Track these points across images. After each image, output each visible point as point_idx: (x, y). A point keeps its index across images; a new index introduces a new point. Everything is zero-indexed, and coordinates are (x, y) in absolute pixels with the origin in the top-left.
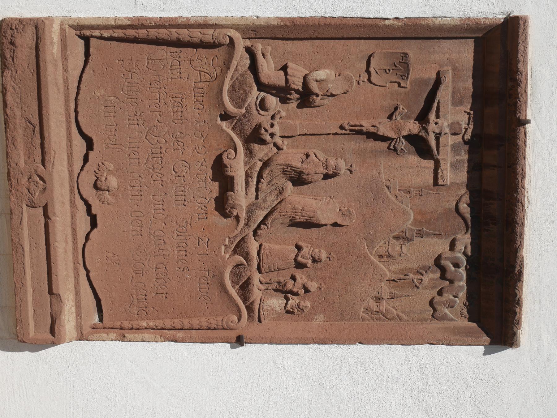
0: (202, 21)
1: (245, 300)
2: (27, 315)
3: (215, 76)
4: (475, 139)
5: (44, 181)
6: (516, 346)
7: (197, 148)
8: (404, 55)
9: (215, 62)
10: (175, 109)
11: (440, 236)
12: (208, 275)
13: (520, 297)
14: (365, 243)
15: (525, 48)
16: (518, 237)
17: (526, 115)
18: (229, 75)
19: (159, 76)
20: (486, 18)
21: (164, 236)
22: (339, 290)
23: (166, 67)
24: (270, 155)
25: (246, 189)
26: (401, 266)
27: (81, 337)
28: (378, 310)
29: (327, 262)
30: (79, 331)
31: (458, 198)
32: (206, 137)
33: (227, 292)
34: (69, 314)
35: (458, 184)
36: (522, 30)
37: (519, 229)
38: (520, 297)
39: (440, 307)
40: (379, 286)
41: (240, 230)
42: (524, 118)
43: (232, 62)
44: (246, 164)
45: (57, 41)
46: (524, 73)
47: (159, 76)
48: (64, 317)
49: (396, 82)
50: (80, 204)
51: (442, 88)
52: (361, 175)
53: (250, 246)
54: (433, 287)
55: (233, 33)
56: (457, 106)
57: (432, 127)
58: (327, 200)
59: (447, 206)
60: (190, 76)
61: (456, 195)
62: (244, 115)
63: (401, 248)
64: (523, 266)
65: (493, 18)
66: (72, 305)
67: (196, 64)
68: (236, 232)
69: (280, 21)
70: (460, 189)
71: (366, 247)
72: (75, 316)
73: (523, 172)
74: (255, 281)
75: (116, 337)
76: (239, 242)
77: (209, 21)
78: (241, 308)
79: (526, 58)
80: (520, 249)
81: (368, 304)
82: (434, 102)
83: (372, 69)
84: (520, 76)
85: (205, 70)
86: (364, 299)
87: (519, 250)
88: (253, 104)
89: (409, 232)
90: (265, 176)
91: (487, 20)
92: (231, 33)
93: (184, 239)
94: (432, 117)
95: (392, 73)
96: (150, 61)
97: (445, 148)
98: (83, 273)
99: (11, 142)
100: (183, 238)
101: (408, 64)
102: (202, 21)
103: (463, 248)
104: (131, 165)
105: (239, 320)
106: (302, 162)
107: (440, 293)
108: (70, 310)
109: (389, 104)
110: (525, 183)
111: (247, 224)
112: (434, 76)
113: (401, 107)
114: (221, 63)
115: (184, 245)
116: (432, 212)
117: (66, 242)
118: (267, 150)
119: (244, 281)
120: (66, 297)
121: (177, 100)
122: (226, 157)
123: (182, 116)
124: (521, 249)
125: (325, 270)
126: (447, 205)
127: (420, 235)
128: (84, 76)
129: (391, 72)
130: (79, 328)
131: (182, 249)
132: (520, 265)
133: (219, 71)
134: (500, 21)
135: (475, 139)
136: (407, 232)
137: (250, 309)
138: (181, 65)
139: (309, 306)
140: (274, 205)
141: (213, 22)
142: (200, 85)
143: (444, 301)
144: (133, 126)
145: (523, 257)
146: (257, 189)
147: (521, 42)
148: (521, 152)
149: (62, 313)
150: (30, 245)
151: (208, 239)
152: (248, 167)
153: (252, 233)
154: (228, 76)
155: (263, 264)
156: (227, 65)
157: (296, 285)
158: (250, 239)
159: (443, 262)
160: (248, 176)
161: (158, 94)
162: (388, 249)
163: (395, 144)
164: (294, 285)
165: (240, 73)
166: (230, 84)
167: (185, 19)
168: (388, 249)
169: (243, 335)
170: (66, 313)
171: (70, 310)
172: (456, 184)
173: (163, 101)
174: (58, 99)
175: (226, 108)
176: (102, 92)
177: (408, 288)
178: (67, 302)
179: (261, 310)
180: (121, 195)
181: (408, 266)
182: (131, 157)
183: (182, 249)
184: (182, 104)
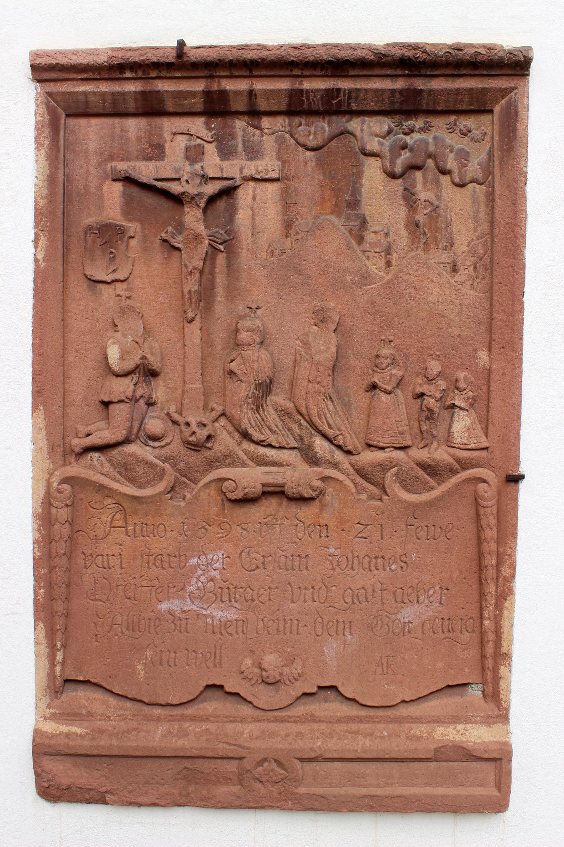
0: (38, 521)
1: (453, 472)
2: (467, 797)
3: (117, 505)
4: (213, 126)
5: (265, 760)
6: (530, 52)
7: (221, 535)
8: (89, 232)
9: (97, 505)
10: (166, 565)
11: (359, 175)
12: (413, 525)
13: (450, 46)
14: (367, 287)
15: (74, 53)
16: (355, 53)
17: (171, 48)
18: (115, 485)
19: (117, 586)
20: (36, 114)
21: (351, 589)
22: (440, 327)
23: (105, 576)
24: (231, 429)
25: (282, 466)
26: (404, 232)
27: (504, 718)
28: (472, 268)
29: (396, 345)
30: (495, 720)
31: (301, 149)
32: (204, 521)
33: (441, 498)
34: (467, 734)
35: (279, 149)
36: (50, 58)
37: (343, 52)
38: (450, 46)
39: (468, 173)
40: (435, 267)
41: (344, 476)
42: (175, 51)
43: (96, 480)
44: (243, 465)
45: (67, 726)
46: (110, 53)
47: (117, 586)
48: (471, 744)
49: (128, 243)
50: (300, 710)
51: (134, 174)
52: (264, 293)
53: (368, 462)
54: (438, 184)
55: (54, 479)
56: (164, 153)
57: (191, 189)
58: (301, 345)
59: (313, 164)
60: (117, 541)
61: (297, 151)
62: (174, 465)
63: (375, 232)
64: (401, 43)
65: (36, 104)
66: (454, 729)
67: (100, 532)
68: (348, 482)
69: (37, 411)
70: (287, 146)
71: (374, 286)
72: (470, 725)
73: (256, 49)
74: (422, 455)
75: (505, 666)
76: (363, 477)
77: (37, 513)
78: (464, 478)
79: (88, 52)
80: (374, 49)
81: (461, 283)
82: (155, 186)
83: (109, 279)
84: (114, 59)
85: (109, 519)
86: (455, 289)
87: (376, 51)
88: (157, 452)
89: (351, 222)
90: (262, 438)
91: (39, 112)
92: (54, 481)
93: (359, 560)
94: (175, 188)
95: (115, 249)
96: (97, 596)
97: (225, 170)
98: (404, 711)
99: (207, 802)
100: (356, 561)
101: (102, 226)
102: (38, 521)
103: (377, 139)
104: (245, 632)
105: (484, 481)
106: (241, 381)
107: (444, 172)
108: (461, 732)
109: (158, 254)
110: (273, 46)
111: (336, 465)
112: (119, 186)
113: (163, 235)
114: (98, 497)
115: (367, 559)
116: (322, 186)
117: (357, 733)
118: (225, 433)
119: (422, 472)
120: (440, 738)
121: (152, 561)
122: (233, 494)
123: (174, 555)
124: (374, 47)
125: (407, 350)
126: (312, 165)
127: (354, 203)
128: (116, 691)
129: (114, 251)
130: (488, 721)
131: (373, 564)
132: (400, 49)
133: (109, 501)
134: (41, 93)
135: (213, 126)
136: (351, 224)
137: (465, 465)
138: (102, 553)
139: (464, 373)
140: (305, 424)
141: (39, 507)
142: (130, 528)
143: (459, 167)
144: (189, 626)
145: (388, 44)
146: (282, 448)
147: (66, 60)
148: (226, 52)
149: (463, 745)
150: (359, 786)
151: (358, 523)
152: (249, 462)
153: (352, 458)
154: (116, 488)
155: (396, 442)
156: (102, 488)
157: (430, 394)
158: (357, 461)
159: (398, 169)
160: (262, 462)
161: (144, 589)
162: (376, 252)
163: (217, 243)
164: (430, 396)
165: (112, 470)
166: (128, 484)
167: (35, 546)
168: (376, 252)
169: (507, 476)
170: (465, 740)
171: (461, 732)
172: (279, 152)
173: (153, 582)
174: (146, 732)
175: (162, 492)
176: (139, 667)
177: (437, 222)
178: (447, 737)
179: (469, 447)
180: (289, 649)
181: (402, 222)
182: (234, 632)
183: (373, 564)
184: (157, 554)
